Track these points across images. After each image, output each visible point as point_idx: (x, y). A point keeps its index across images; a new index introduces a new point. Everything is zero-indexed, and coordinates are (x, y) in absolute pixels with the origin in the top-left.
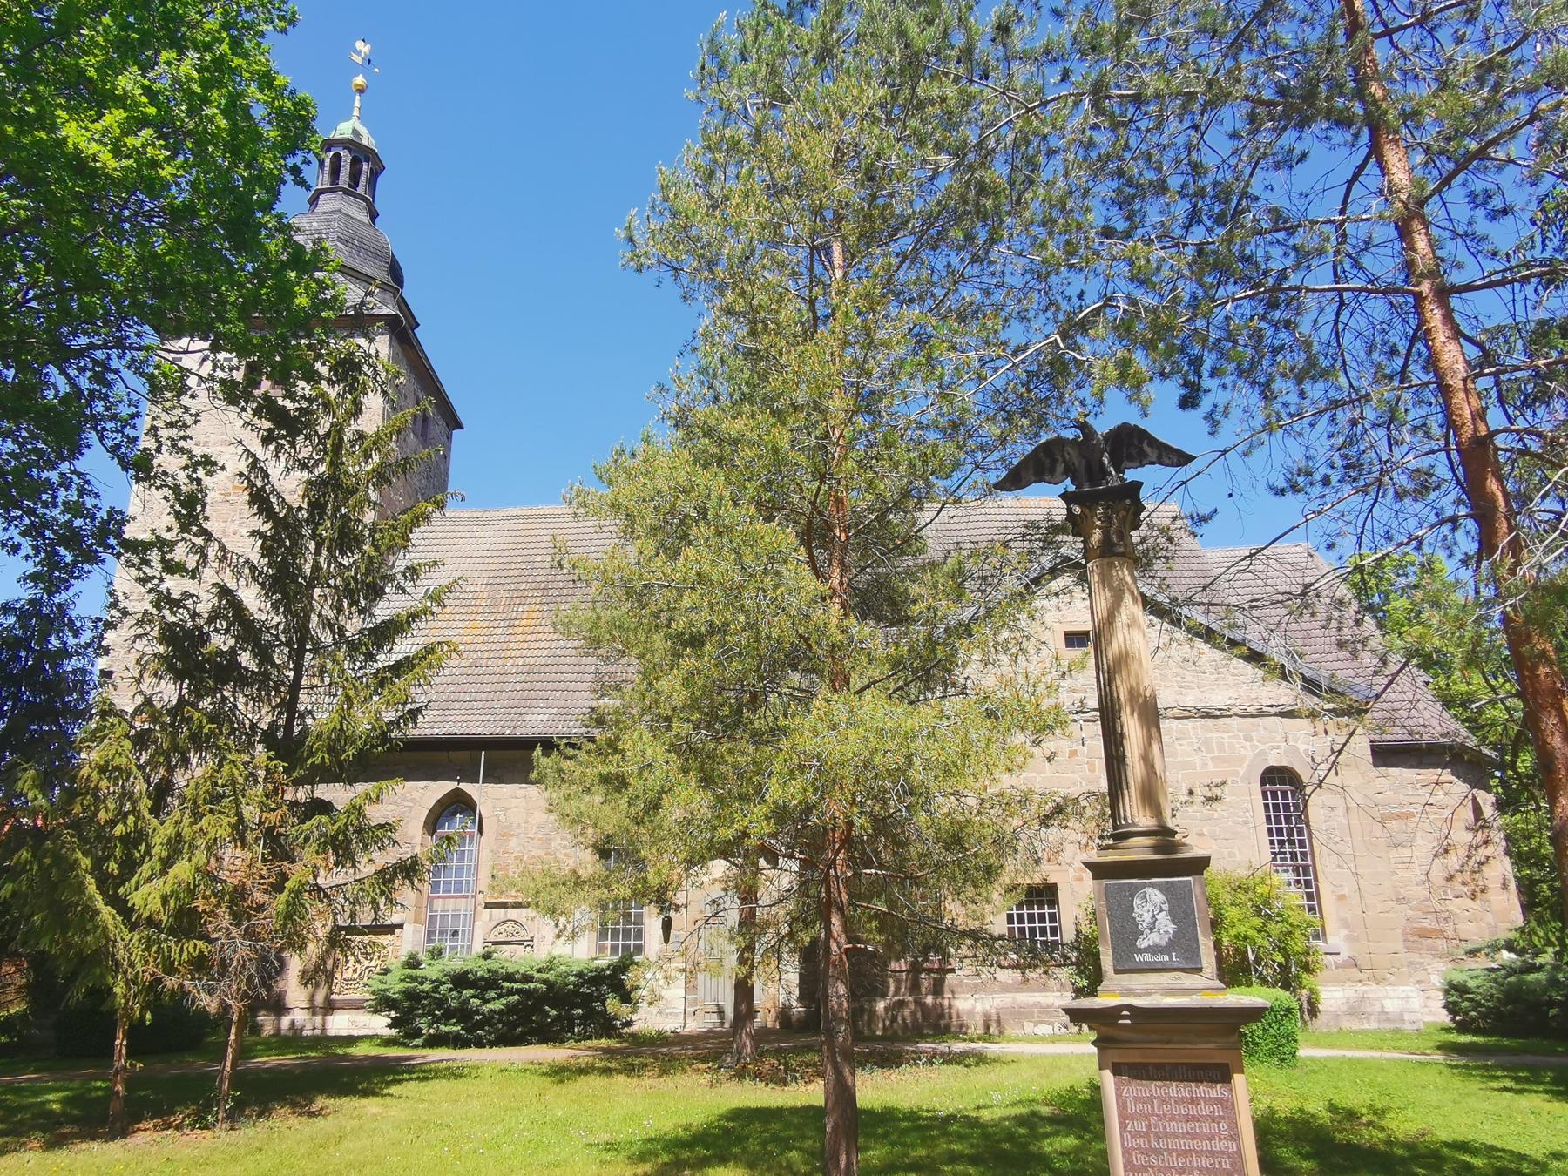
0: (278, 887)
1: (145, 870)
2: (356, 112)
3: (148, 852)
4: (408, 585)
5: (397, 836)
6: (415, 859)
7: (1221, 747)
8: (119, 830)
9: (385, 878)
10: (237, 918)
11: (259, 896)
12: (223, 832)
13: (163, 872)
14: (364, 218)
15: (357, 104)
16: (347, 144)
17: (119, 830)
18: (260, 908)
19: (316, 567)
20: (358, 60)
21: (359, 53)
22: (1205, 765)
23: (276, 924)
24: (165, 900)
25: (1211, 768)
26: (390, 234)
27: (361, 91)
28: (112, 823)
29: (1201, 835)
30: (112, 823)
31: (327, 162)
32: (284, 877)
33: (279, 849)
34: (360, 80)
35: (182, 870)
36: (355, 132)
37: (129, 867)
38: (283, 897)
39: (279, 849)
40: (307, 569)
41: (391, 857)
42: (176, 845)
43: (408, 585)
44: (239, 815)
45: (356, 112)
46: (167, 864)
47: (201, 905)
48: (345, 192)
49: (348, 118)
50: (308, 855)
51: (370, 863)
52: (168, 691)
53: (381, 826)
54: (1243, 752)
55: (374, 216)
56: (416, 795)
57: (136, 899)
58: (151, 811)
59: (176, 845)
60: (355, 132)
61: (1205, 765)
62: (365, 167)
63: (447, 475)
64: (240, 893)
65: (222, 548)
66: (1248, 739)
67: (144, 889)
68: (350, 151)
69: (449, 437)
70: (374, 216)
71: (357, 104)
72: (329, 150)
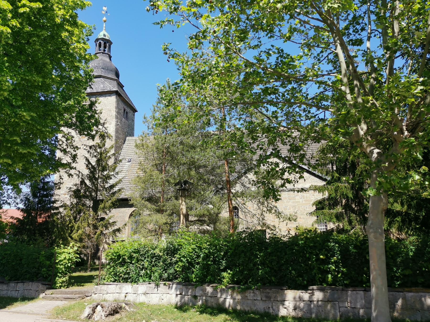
0: (95, 234)
1: (74, 232)
2: (104, 28)
3: (74, 229)
4: (116, 176)
5: (117, 224)
6: (119, 228)
7: (307, 197)
8: (70, 225)
9: (114, 231)
10: (89, 239)
11: (92, 236)
12: (86, 225)
13: (77, 232)
14: (108, 60)
15: (104, 26)
16: (103, 39)
17: (70, 225)
18: (93, 237)
19: (99, 176)
20: (103, 12)
21: (104, 11)
22: (302, 202)
23: (95, 240)
24: (78, 236)
25: (304, 202)
26: (115, 63)
27: (105, 21)
28: (69, 224)
29: (300, 218)
30: (69, 224)
31: (98, 45)
32: (96, 232)
33: (95, 227)
34: (104, 19)
35: (80, 232)
36: (104, 35)
37: (72, 231)
38: (96, 236)
39: (95, 227)
40: (97, 177)
41: (116, 227)
42: (79, 228)
43: (116, 176)
44: (88, 222)
45: (104, 28)
46: (78, 231)
47: (83, 237)
48: (103, 53)
49: (102, 31)
50: (100, 228)
51: (111, 229)
52: (75, 201)
53: (113, 222)
54: (312, 199)
55: (110, 57)
56: (127, 211)
57: (73, 236)
58: (74, 222)
59: (79, 228)
60: (104, 35)
61: (302, 202)
62: (107, 45)
63: (134, 125)
64: (89, 235)
65: (82, 174)
66: (313, 195)
67: (75, 235)
68: (103, 41)
69: (134, 115)
70: (110, 57)
71: (104, 26)
72: (98, 41)
